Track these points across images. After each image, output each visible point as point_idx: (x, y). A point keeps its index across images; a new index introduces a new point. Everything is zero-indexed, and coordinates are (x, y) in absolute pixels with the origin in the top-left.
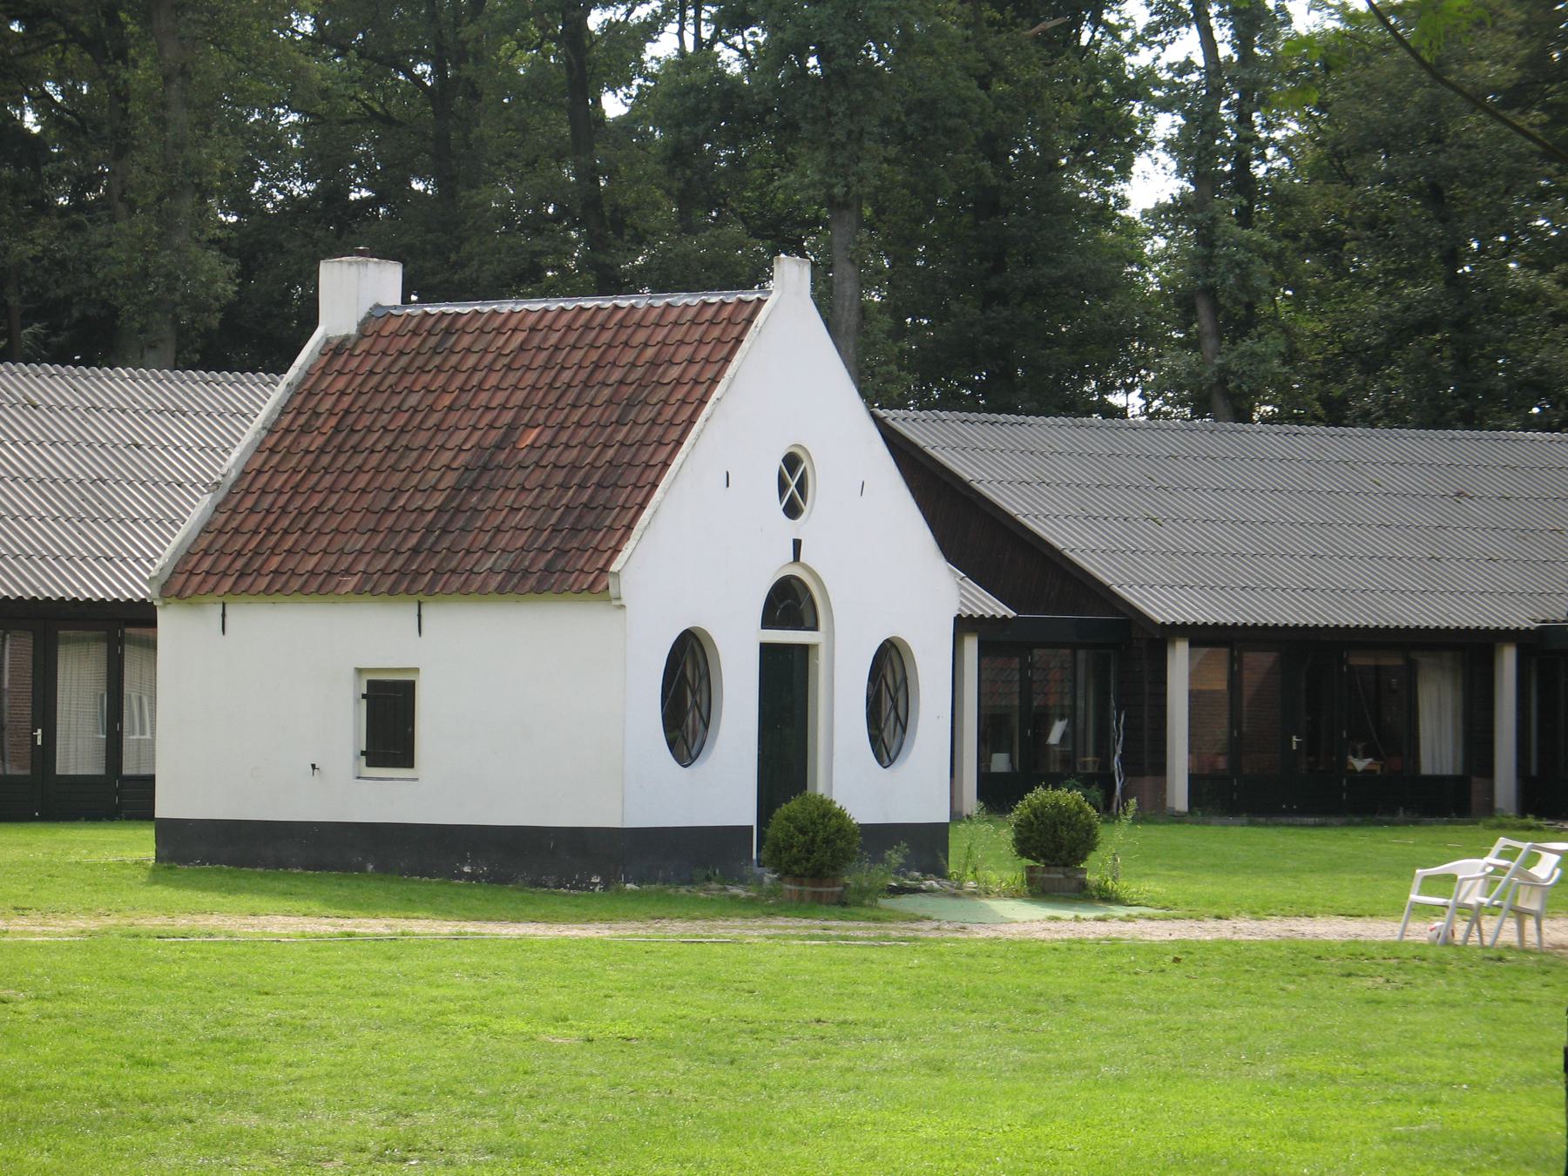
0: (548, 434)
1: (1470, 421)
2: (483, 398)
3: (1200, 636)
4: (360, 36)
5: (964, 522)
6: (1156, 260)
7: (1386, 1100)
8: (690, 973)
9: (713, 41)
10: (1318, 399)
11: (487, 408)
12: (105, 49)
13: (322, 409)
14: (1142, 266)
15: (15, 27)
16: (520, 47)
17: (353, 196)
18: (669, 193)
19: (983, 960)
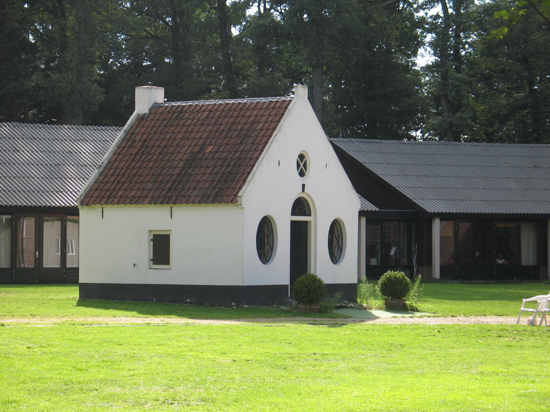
0: (216, 147)
1: (538, 141)
2: (193, 135)
3: (444, 217)
4: (146, 8)
5: (362, 179)
6: (426, 85)
7: (517, 381)
8: (269, 337)
9: (270, 9)
10: (484, 133)
11: (194, 139)
12: (58, 14)
13: (136, 139)
14: (421, 87)
15: (26, 6)
16: (202, 11)
17: (144, 64)
18: (255, 62)
19: (371, 332)
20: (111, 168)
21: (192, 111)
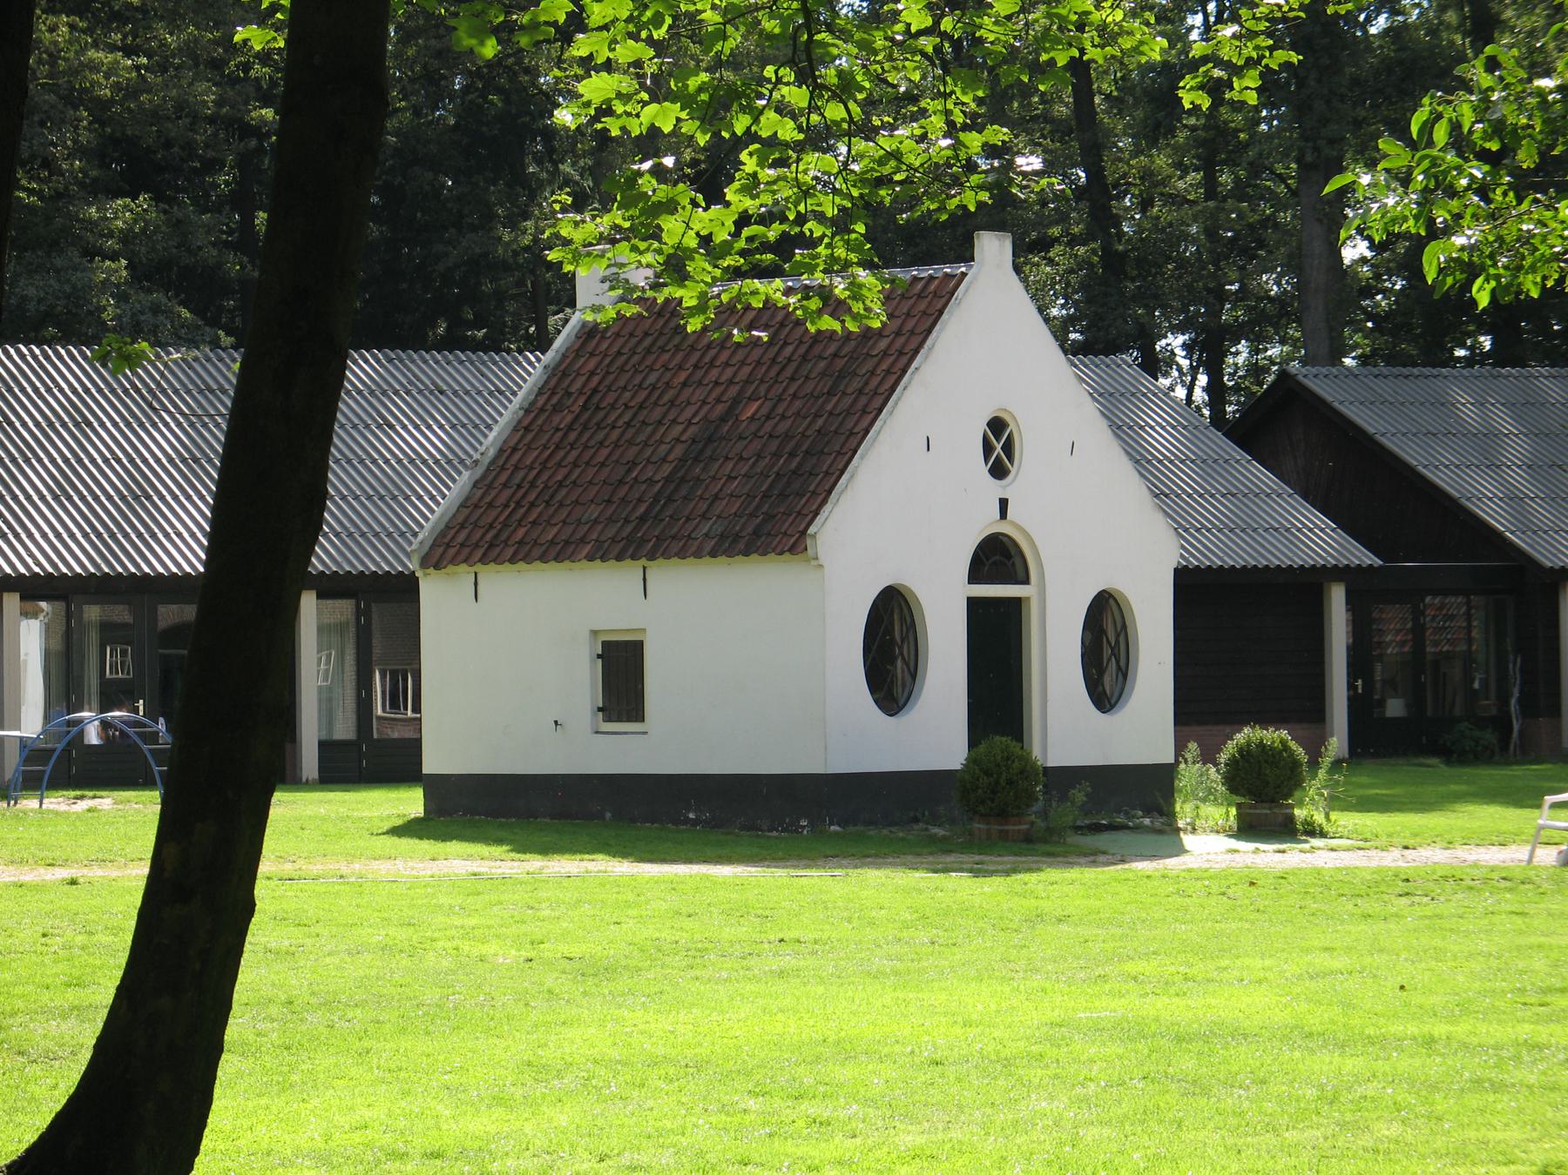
0: (769, 404)
11: (717, 383)
20: (503, 468)
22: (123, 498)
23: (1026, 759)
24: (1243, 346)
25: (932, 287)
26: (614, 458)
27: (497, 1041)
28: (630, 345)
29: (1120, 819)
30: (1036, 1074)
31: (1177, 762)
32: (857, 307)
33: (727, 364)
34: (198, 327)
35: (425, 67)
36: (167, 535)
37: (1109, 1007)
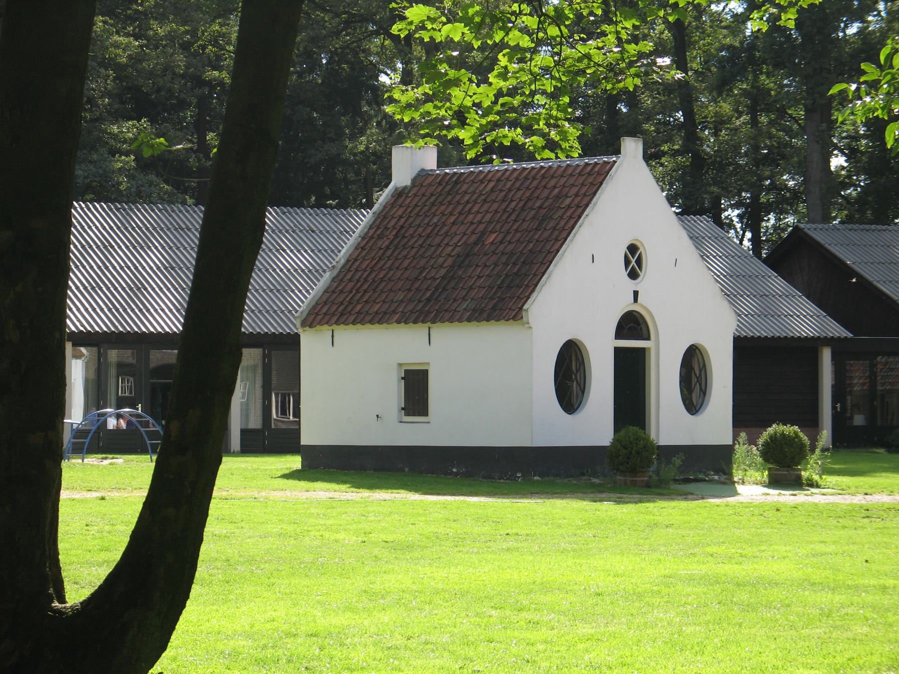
0: (502, 235)
11: (472, 223)
13: (389, 226)
20: (349, 270)
21: (473, 181)
22: (131, 289)
23: (647, 439)
24: (772, 216)
25: (596, 169)
26: (413, 265)
27: (346, 580)
28: (422, 201)
29: (701, 476)
30: (656, 600)
31: (734, 444)
32: (565, 145)
33: (478, 212)
34: (174, 194)
35: (305, 48)
36: (156, 310)
37: (698, 569)
